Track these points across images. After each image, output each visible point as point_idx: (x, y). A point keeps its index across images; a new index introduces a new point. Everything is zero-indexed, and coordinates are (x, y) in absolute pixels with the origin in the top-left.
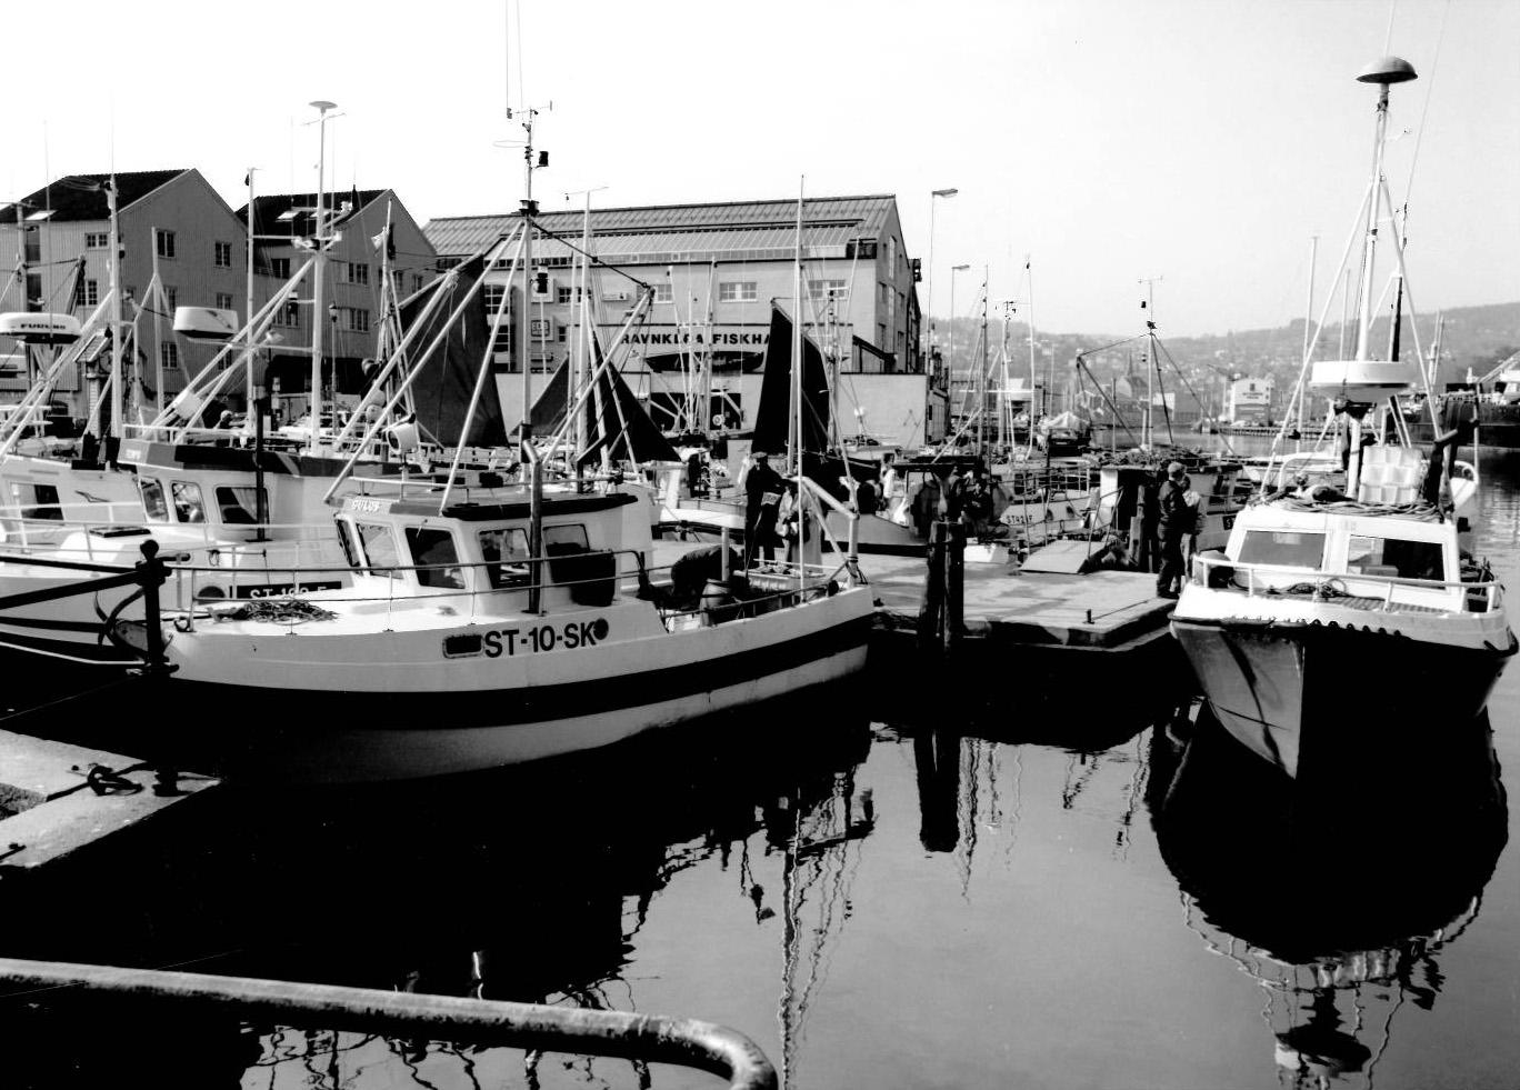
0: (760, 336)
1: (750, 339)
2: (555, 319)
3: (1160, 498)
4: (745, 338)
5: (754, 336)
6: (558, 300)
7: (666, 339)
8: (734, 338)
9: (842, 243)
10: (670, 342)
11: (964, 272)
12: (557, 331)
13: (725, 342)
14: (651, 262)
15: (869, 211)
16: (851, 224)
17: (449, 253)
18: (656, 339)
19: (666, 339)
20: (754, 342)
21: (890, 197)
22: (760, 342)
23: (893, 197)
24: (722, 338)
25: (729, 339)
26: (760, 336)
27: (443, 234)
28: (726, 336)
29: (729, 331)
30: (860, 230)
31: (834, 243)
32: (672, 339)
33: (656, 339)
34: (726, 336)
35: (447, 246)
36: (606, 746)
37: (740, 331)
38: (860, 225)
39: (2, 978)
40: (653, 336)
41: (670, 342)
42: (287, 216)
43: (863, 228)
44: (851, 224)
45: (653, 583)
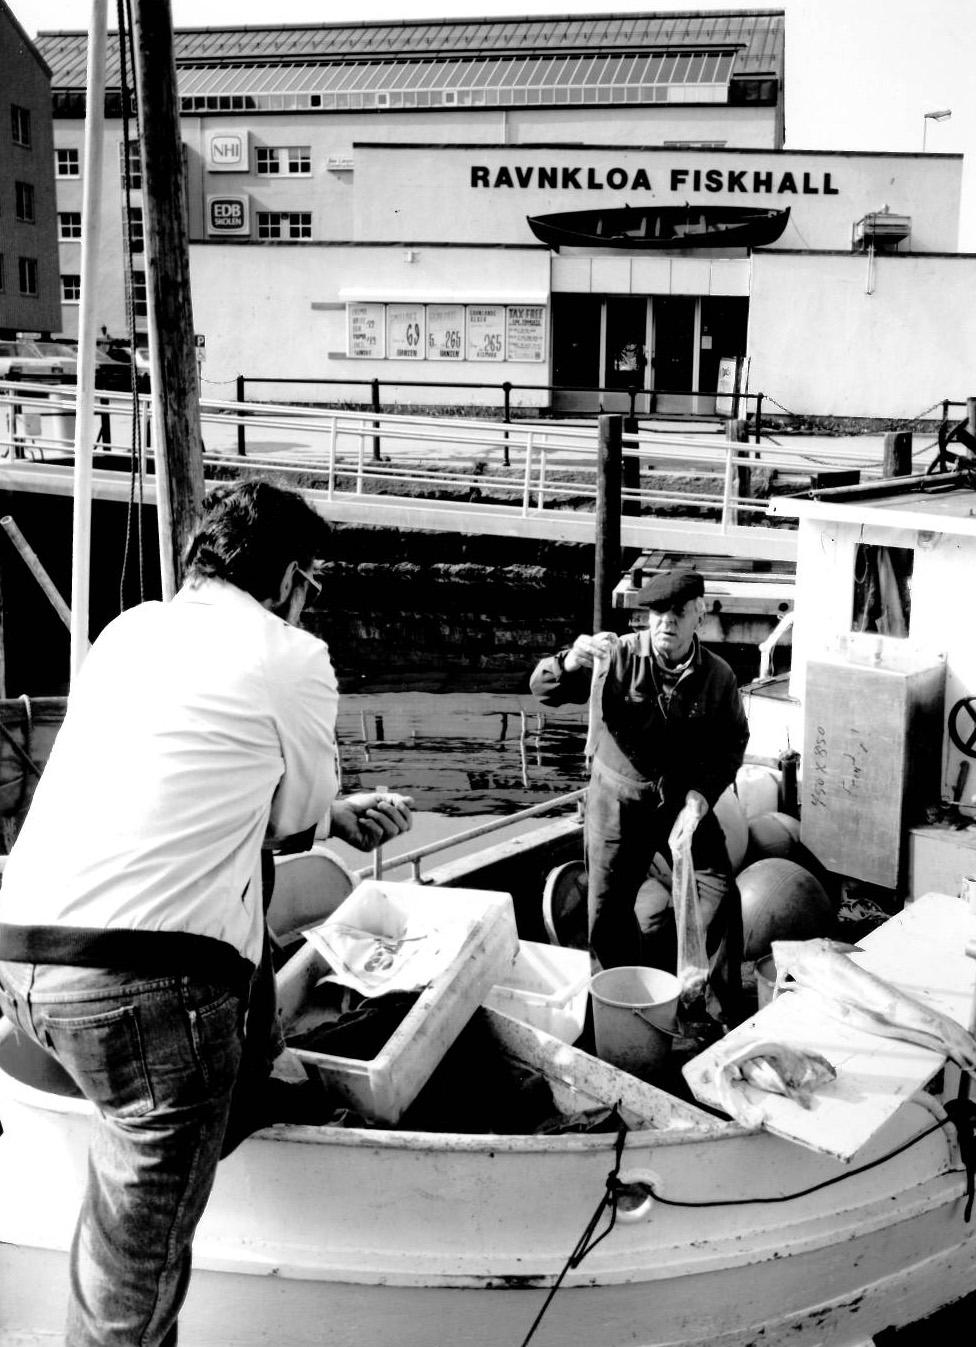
0: (769, 175)
1: (748, 181)
2: (251, 200)
3: (970, 457)
4: (735, 180)
5: (757, 175)
6: (255, 168)
7: (570, 177)
8: (714, 180)
9: (720, 78)
10: (577, 186)
11: (944, 123)
12: (256, 219)
13: (697, 187)
14: (408, 105)
15: (750, 32)
16: (729, 51)
17: (72, 85)
18: (547, 178)
19: (570, 177)
20: (756, 190)
21: (771, 15)
22: (769, 190)
23: (782, 13)
24: (690, 179)
25: (704, 181)
26: (769, 175)
27: (60, 56)
28: (697, 174)
29: (706, 163)
30: (745, 59)
31: (707, 78)
32: (582, 178)
33: (547, 178)
34: (697, 174)
35: (68, 73)
36: (402, 1020)
37: (725, 164)
38: (742, 52)
39: (3, 492)
40: (542, 171)
41: (577, 186)
42: (171, 436)
43: (747, 56)
44: (729, 51)
45: (970, 1098)
